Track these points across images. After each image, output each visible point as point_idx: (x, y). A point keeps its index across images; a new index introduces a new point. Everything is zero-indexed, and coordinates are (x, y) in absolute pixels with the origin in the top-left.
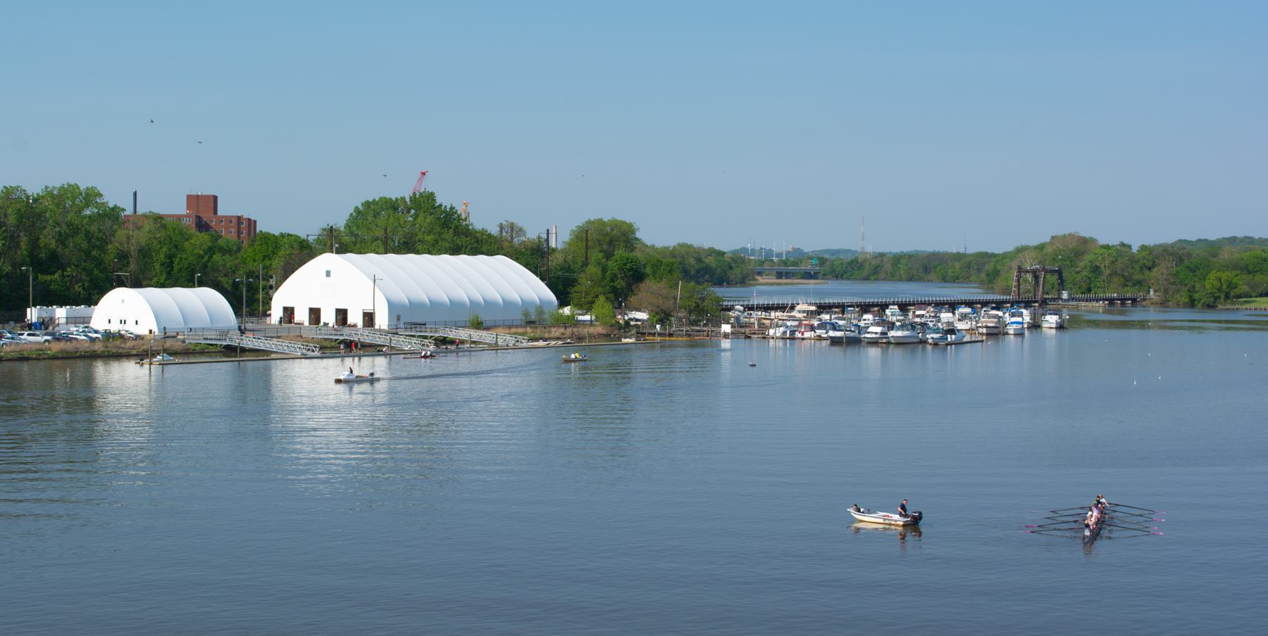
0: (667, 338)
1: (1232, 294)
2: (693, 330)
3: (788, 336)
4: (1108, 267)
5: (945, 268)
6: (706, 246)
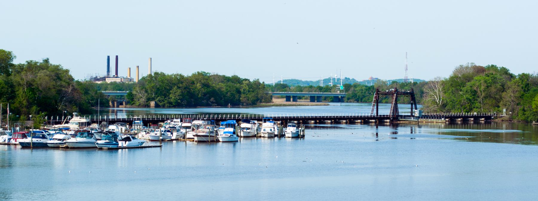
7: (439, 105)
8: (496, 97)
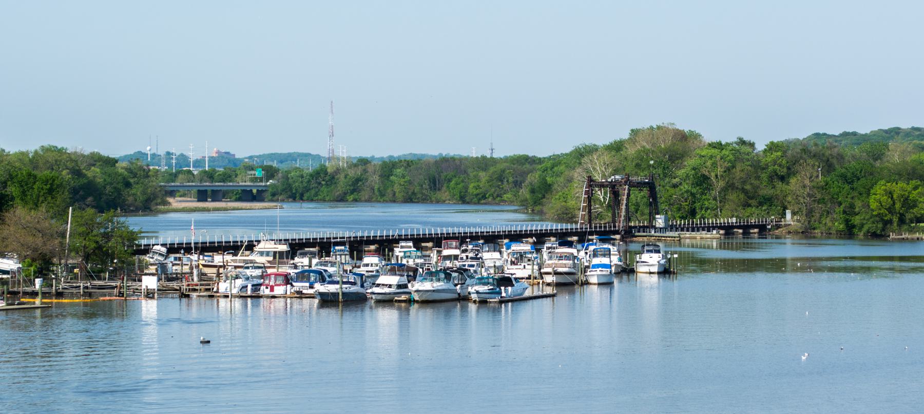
0: (55, 301)
1: (908, 216)
2: (94, 287)
3: (249, 293)
4: (722, 176)
5: (463, 181)
6: (87, 151)
8: (746, 187)
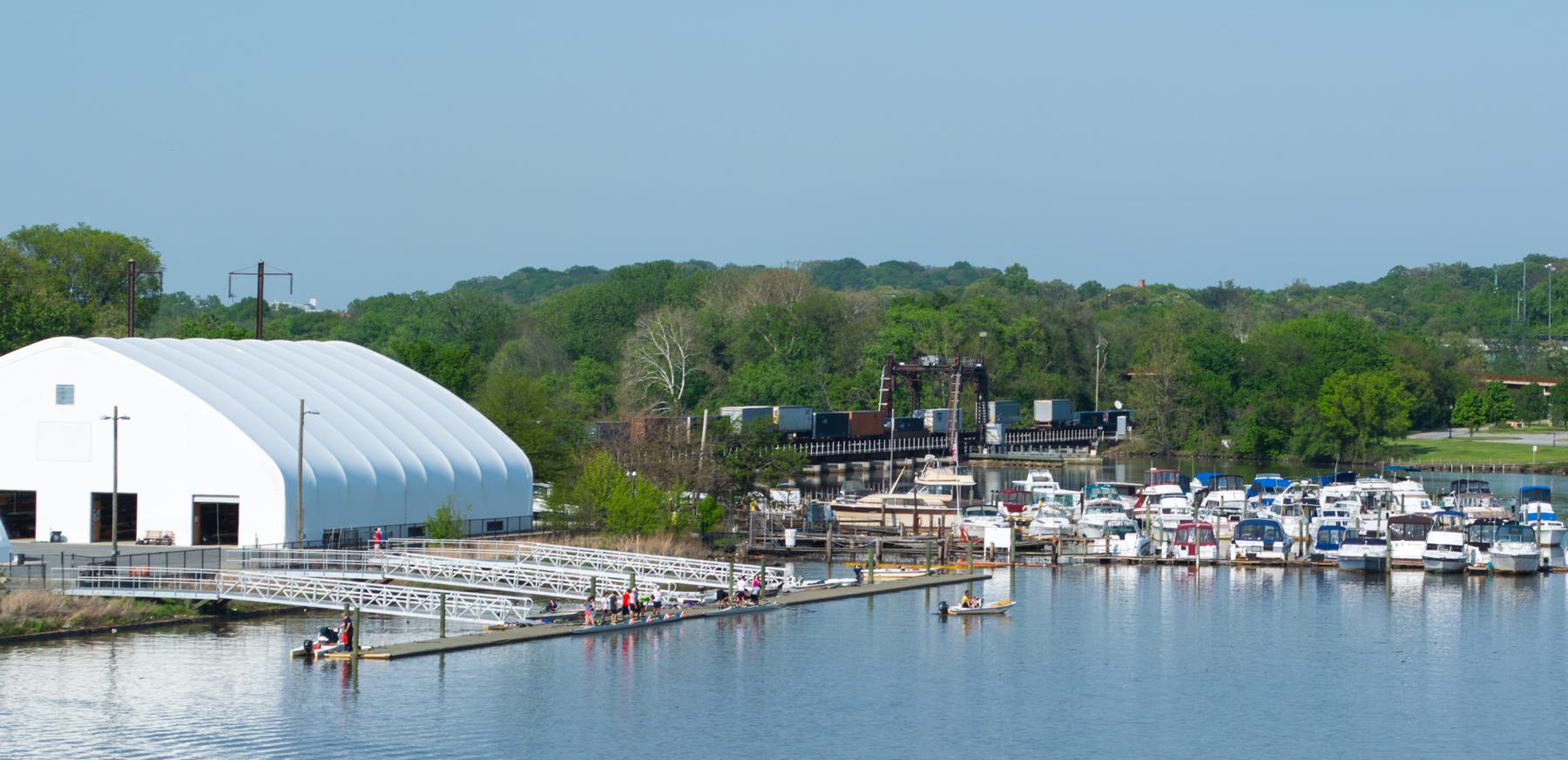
7: (675, 401)
